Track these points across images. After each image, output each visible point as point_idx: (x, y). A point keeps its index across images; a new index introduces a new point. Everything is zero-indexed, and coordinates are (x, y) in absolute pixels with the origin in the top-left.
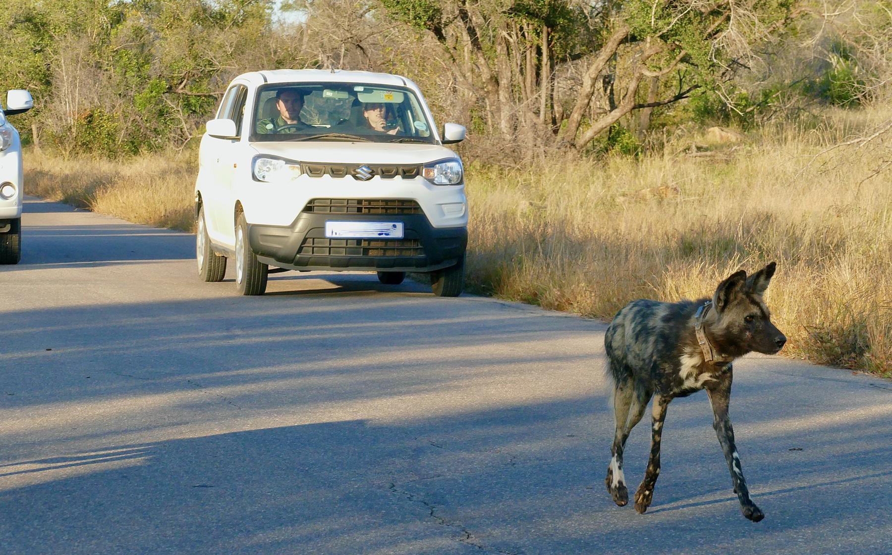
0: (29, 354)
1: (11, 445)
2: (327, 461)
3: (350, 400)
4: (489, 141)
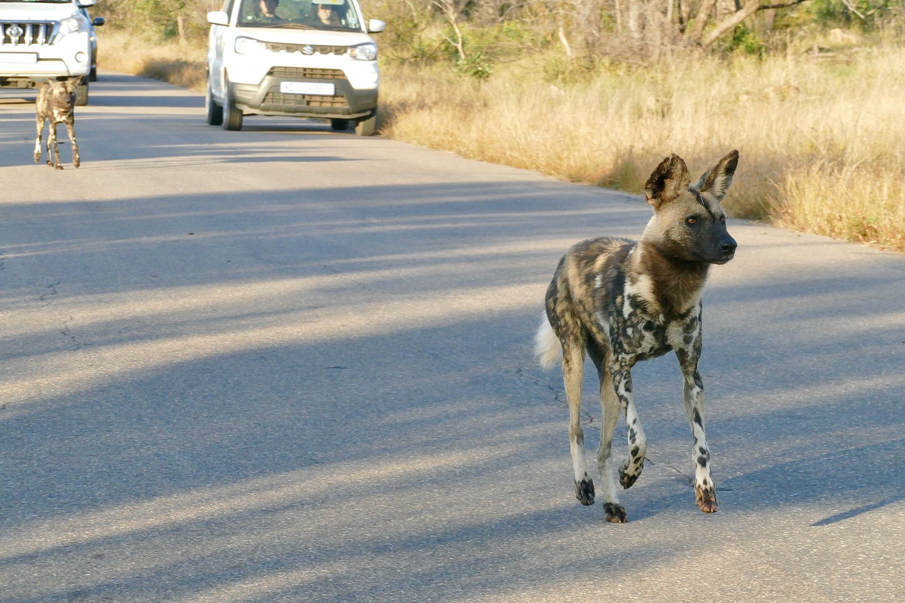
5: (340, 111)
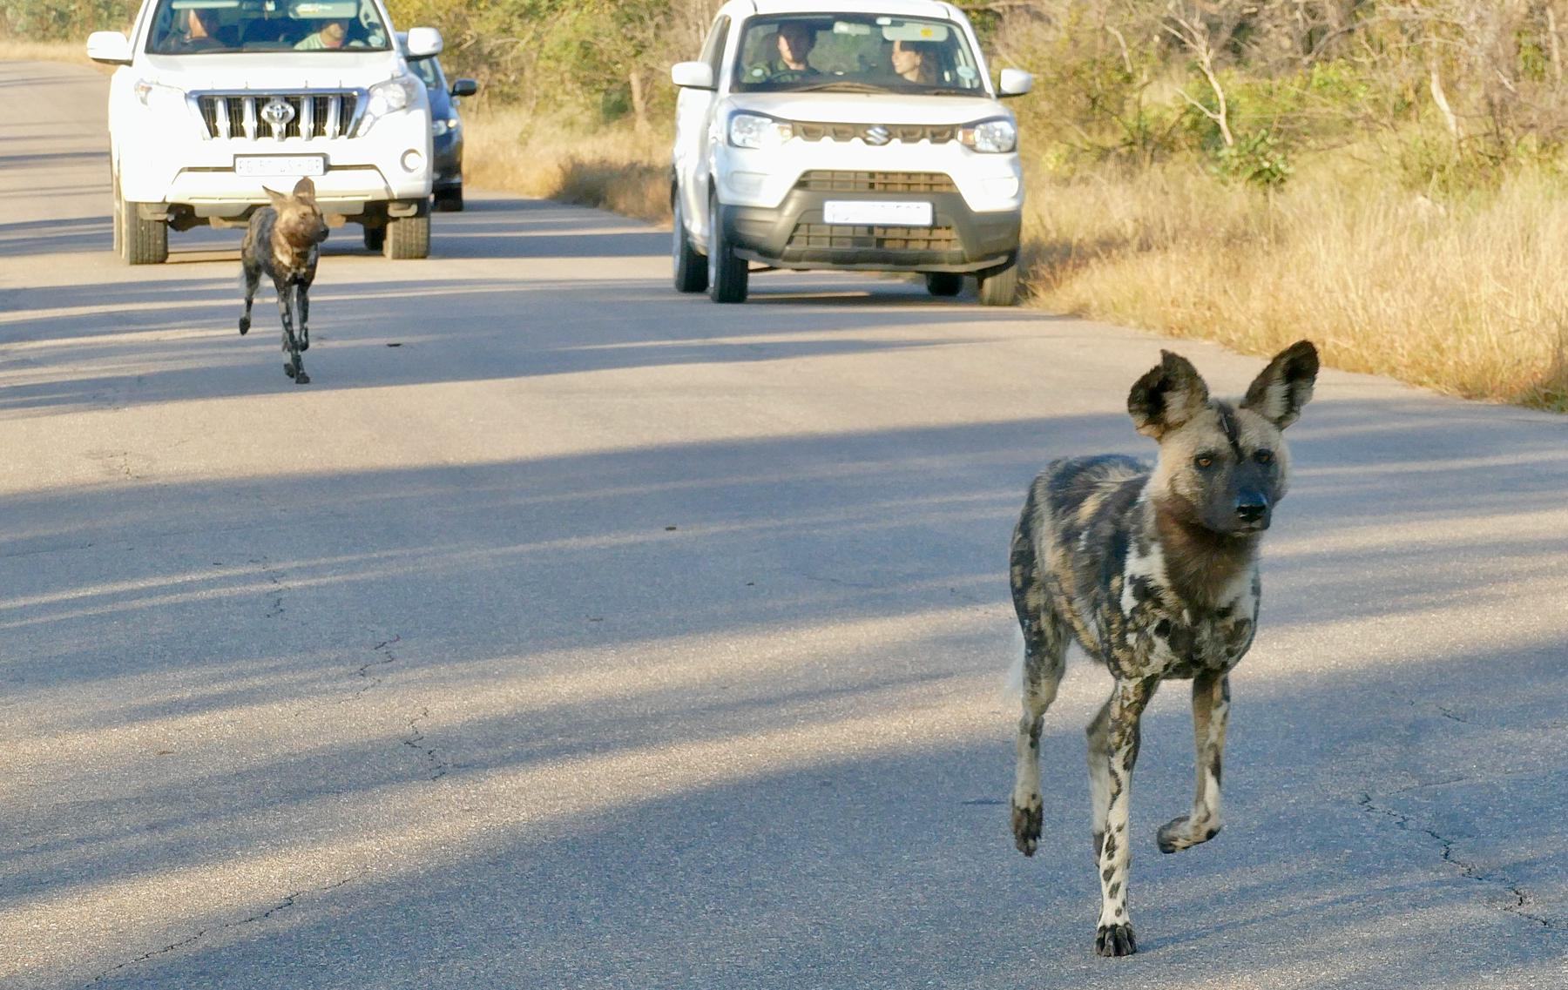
0: (632, 538)
1: (597, 721)
2: (1233, 751)
3: (1278, 626)
4: (1554, 95)
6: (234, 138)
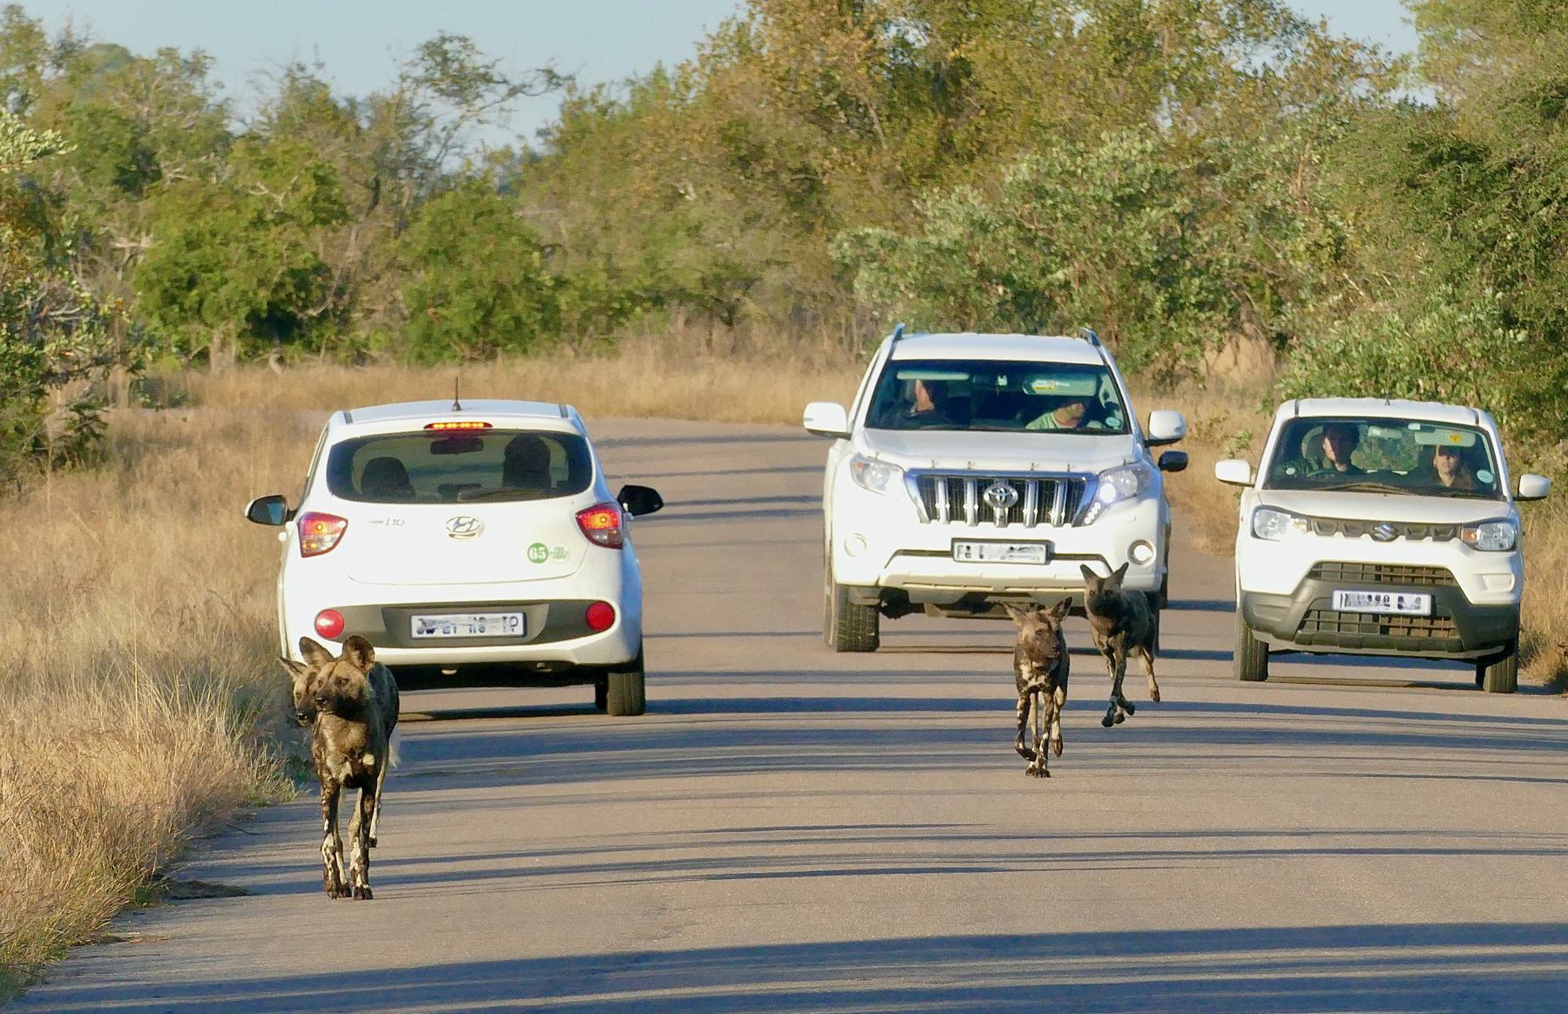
5: (1444, 645)
6: (953, 522)
